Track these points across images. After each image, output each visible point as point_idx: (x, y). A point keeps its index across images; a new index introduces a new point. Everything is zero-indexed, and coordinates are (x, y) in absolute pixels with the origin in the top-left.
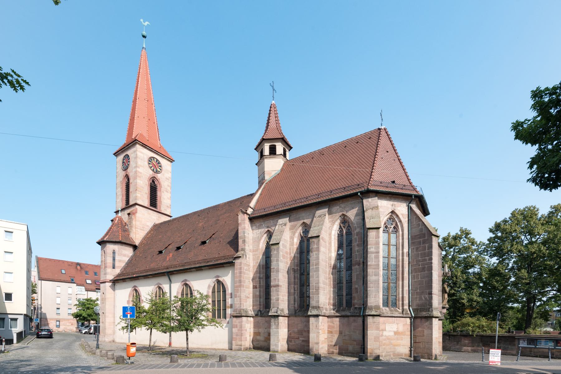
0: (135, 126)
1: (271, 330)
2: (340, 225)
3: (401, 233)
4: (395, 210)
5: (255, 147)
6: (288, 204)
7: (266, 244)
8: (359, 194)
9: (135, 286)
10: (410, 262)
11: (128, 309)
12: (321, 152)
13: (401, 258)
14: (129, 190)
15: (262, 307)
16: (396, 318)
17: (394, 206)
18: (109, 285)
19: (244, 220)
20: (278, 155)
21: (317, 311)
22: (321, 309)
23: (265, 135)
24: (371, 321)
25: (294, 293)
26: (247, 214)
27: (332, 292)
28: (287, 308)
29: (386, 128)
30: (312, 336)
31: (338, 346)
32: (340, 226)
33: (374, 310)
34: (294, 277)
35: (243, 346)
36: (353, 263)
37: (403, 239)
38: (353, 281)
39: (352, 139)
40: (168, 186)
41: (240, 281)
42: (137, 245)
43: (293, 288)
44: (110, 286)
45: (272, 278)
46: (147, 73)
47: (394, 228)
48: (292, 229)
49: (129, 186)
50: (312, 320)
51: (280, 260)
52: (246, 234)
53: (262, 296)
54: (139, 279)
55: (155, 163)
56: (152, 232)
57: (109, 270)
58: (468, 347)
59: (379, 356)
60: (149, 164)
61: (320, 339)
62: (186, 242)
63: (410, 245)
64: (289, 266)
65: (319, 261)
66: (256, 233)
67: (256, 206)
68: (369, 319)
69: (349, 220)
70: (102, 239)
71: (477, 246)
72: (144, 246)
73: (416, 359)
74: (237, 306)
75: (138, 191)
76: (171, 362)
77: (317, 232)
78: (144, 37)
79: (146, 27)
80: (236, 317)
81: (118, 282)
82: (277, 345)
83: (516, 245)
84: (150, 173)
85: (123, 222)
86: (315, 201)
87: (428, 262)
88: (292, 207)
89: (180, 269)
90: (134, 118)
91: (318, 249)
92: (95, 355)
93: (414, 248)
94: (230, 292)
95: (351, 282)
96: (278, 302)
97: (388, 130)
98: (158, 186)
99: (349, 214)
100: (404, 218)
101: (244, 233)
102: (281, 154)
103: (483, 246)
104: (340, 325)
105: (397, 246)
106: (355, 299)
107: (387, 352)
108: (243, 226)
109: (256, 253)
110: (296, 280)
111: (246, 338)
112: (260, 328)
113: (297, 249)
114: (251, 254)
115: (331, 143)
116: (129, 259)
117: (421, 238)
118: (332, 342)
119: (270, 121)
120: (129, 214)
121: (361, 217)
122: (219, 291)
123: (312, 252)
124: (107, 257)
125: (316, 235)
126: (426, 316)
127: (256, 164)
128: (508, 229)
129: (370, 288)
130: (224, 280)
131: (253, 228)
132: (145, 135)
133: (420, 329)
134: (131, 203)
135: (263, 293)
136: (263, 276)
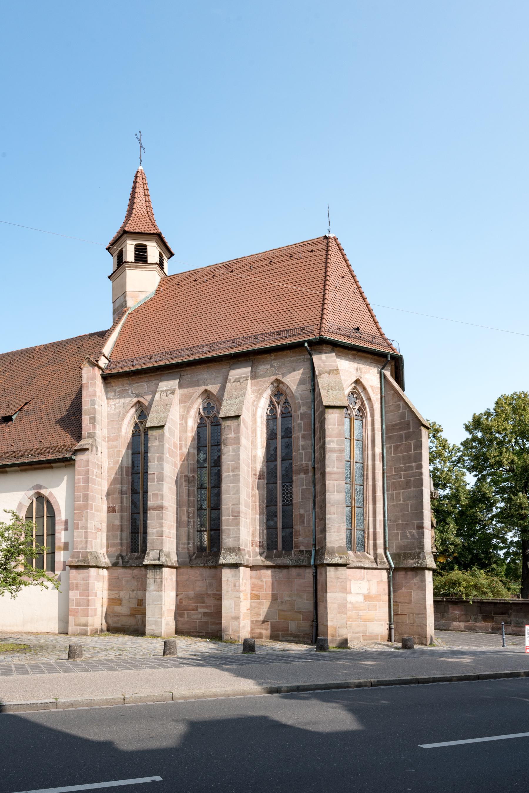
1: (147, 593)
2: (271, 398)
3: (369, 419)
4: (361, 377)
5: (108, 245)
7: (132, 428)
8: (306, 345)
10: (385, 471)
12: (227, 266)
13: (370, 463)
15: (124, 548)
16: (366, 571)
17: (359, 371)
19: (94, 378)
20: (150, 264)
21: (236, 556)
22: (243, 552)
24: (333, 576)
25: (188, 522)
26: (99, 367)
29: (337, 237)
30: (227, 604)
31: (270, 623)
32: (271, 401)
33: (337, 555)
34: (187, 491)
35: (91, 625)
36: (295, 467)
37: (373, 430)
38: (294, 502)
39: (280, 250)
41: (86, 497)
43: (186, 513)
47: (359, 410)
48: (185, 402)
50: (226, 573)
52: (96, 407)
53: (125, 527)
58: (459, 621)
59: (346, 641)
63: (384, 440)
64: (178, 470)
65: (239, 463)
66: (115, 405)
67: (112, 353)
68: (330, 571)
69: (288, 391)
71: (449, 452)
73: (406, 645)
74: (80, 546)
77: (234, 408)
80: (77, 567)
82: (158, 623)
83: (506, 452)
87: (416, 472)
88: (185, 360)
93: (390, 447)
94: (63, 518)
95: (292, 504)
96: (162, 539)
97: (339, 241)
99: (288, 380)
100: (374, 393)
101: (93, 403)
102: (156, 264)
103: (459, 452)
104: (273, 584)
105: (364, 441)
106: (300, 535)
107: (353, 633)
108: (90, 389)
109: (115, 443)
110: (192, 498)
111: (96, 609)
112: (122, 590)
113: (193, 440)
114: (105, 444)
115: (246, 253)
117: (402, 430)
121: (309, 387)
122: (40, 517)
123: (226, 445)
125: (233, 415)
126: (414, 567)
127: (109, 277)
128: (495, 427)
129: (330, 514)
130: (51, 493)
133: (404, 590)
135: (127, 521)
136: (128, 488)
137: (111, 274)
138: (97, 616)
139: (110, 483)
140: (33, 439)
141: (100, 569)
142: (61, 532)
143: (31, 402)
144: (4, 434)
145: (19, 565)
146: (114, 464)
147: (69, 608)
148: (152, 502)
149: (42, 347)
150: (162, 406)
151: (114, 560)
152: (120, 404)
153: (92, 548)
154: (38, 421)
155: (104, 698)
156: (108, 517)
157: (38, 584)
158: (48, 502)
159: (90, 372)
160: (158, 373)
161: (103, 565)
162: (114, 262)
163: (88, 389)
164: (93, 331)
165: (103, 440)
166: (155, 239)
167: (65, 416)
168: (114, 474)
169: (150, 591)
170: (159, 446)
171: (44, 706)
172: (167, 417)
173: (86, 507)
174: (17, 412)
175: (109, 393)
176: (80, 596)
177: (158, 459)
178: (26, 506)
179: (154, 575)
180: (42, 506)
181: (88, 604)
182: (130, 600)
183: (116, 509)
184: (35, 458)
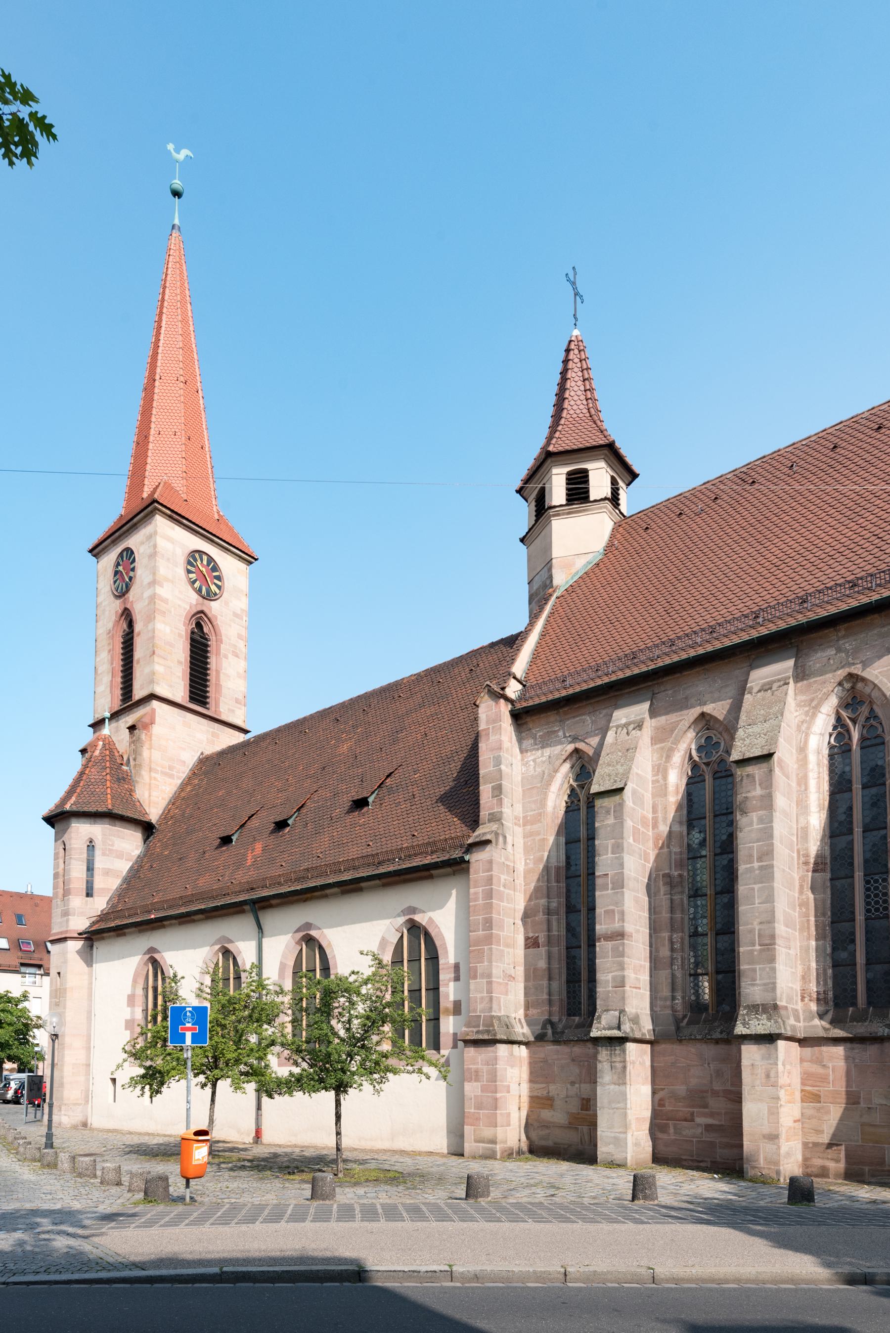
0: (149, 460)
2: (838, 713)
5: (518, 484)
6: (643, 658)
7: (566, 798)
9: (152, 950)
11: (185, 1014)
14: (132, 656)
15: (556, 1009)
18: (74, 946)
19: (498, 719)
20: (595, 501)
21: (769, 1019)
22: (783, 1012)
23: (554, 441)
25: (672, 959)
26: (507, 699)
27: (813, 955)
28: (649, 1012)
31: (843, 1148)
32: (839, 719)
34: (668, 902)
35: (502, 1142)
39: (855, 420)
40: (240, 637)
41: (489, 924)
42: (154, 821)
43: (667, 942)
44: (78, 952)
45: (599, 911)
46: (183, 302)
48: (662, 741)
49: (132, 644)
51: (625, 845)
52: (503, 767)
54: (164, 927)
55: (204, 570)
56: (196, 781)
57: (77, 901)
60: (189, 572)
61: (781, 1120)
62: (302, 806)
64: (650, 866)
65: (772, 844)
66: (534, 760)
67: (528, 672)
69: (875, 694)
70: (57, 806)
72: (174, 824)
75: (159, 656)
76: (313, 1196)
77: (761, 741)
78: (177, 194)
79: (181, 164)
80: (476, 1043)
81: (103, 939)
82: (620, 1143)
84: (190, 599)
85: (117, 754)
86: (745, 637)
89: (293, 889)
90: (147, 437)
91: (768, 802)
92: (54, 1171)
96: (624, 992)
98: (213, 638)
99: (876, 672)
101: (498, 761)
102: (606, 499)
104: (848, 1073)
108: (493, 738)
109: (536, 827)
110: (678, 916)
111: (509, 1114)
113: (679, 808)
114: (519, 830)
116: (132, 867)
118: (819, 1132)
119: (567, 395)
120: (132, 728)
122: (414, 960)
123: (744, 813)
124: (73, 862)
127: (522, 540)
131: (524, 747)
132: (179, 485)
134: (138, 693)
135: (560, 960)
136: (559, 903)
138: (511, 1127)
139: (528, 897)
140: (401, 832)
141: (514, 1046)
143: (397, 771)
146: (534, 864)
147: (463, 1112)
148: (603, 926)
150: (620, 754)
151: (538, 1029)
152: (544, 759)
153: (500, 1010)
155: (531, 1270)
156: (526, 956)
158: (427, 935)
159: (492, 709)
160: (612, 694)
163: (489, 738)
164: (495, 639)
165: (516, 824)
167: (451, 788)
168: (535, 880)
169: (603, 1085)
171: (431, 1277)
172: (629, 772)
173: (489, 940)
174: (376, 790)
176: (482, 1091)
177: (613, 848)
178: (393, 943)
182: (567, 1099)
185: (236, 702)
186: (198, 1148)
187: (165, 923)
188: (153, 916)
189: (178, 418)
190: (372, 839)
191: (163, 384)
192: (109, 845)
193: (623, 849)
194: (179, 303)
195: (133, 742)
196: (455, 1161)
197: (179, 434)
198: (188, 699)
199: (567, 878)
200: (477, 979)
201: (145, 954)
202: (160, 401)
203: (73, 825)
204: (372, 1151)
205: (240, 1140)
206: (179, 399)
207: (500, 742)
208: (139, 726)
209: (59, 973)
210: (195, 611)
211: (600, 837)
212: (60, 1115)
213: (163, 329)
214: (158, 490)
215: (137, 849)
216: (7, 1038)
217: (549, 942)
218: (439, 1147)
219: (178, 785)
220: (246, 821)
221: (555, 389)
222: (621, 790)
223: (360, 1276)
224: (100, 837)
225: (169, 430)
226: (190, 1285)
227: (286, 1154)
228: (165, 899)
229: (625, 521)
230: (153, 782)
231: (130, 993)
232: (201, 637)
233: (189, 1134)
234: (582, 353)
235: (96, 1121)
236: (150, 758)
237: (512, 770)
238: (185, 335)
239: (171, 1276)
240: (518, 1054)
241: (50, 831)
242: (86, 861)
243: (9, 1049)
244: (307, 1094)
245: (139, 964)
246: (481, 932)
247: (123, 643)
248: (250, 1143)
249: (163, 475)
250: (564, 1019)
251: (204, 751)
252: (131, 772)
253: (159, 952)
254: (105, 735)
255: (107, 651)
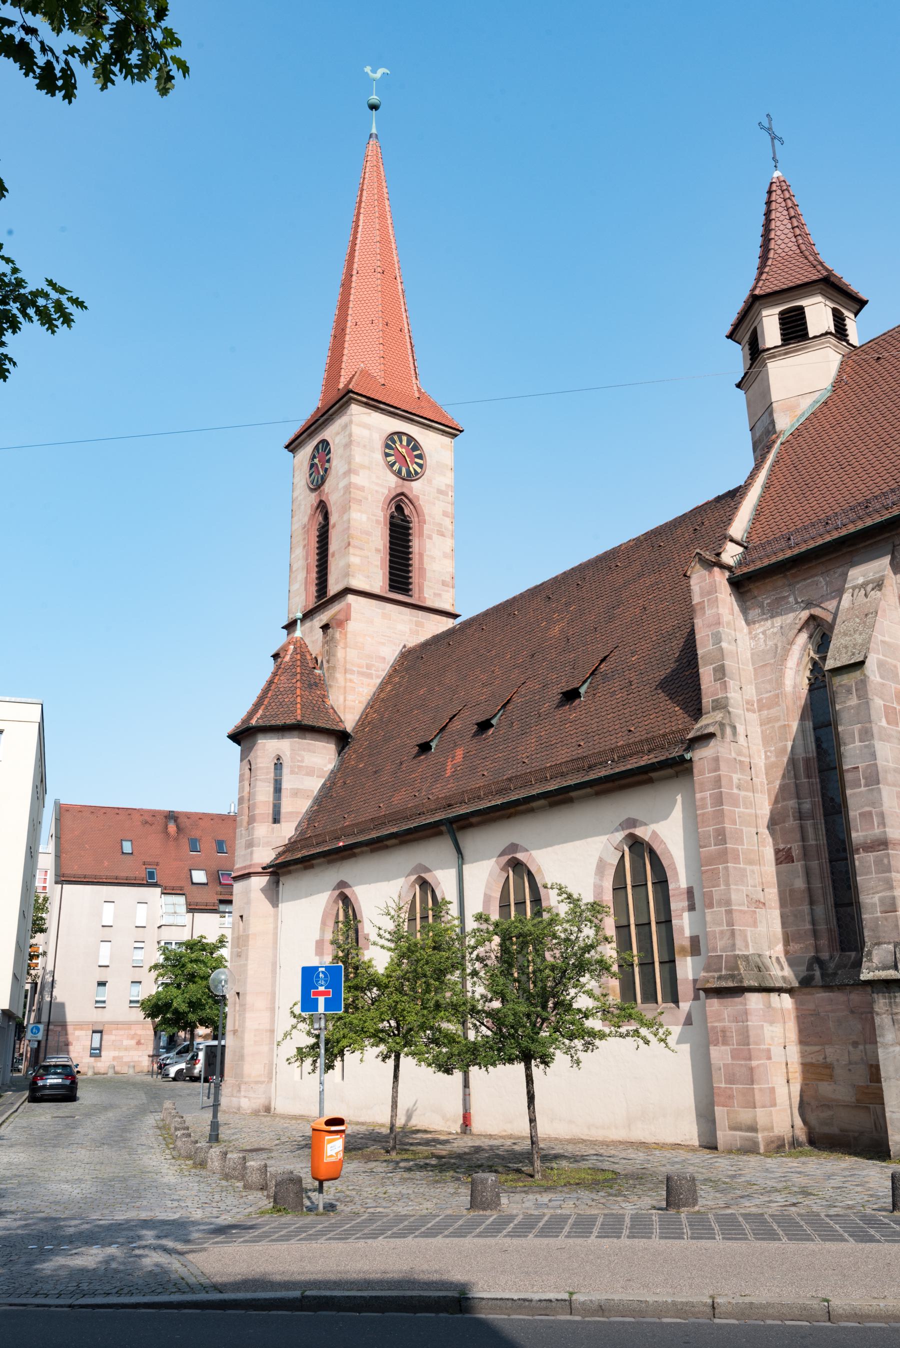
0: (346, 352)
5: (728, 329)
6: (878, 506)
7: (808, 673)
11: (318, 976)
14: (327, 550)
15: (824, 942)
18: (259, 882)
19: (713, 590)
26: (723, 566)
35: (765, 1129)
40: (445, 514)
41: (721, 836)
42: (349, 729)
44: (262, 890)
46: (381, 200)
51: (875, 730)
52: (724, 645)
53: (818, 894)
55: (403, 451)
60: (387, 455)
66: (764, 633)
72: (371, 731)
74: (720, 944)
75: (355, 547)
78: (374, 107)
81: (290, 872)
85: (308, 657)
89: (493, 803)
90: (344, 330)
94: (683, 884)
98: (415, 519)
102: (827, 333)
108: (709, 612)
109: (774, 712)
111: (772, 1090)
114: (753, 717)
116: (324, 784)
120: (325, 627)
122: (639, 886)
124: (259, 783)
127: (739, 386)
130: (654, 833)
132: (376, 371)
134: (333, 588)
135: (822, 878)
136: (813, 804)
137: (740, 379)
138: (778, 1108)
139: (773, 798)
140: (616, 727)
141: (772, 994)
142: (682, 915)
143: (613, 654)
144: (567, 726)
145: (581, 994)
146: (777, 757)
147: (712, 1088)
148: (860, 834)
149: (631, 544)
150: (857, 620)
151: (803, 970)
152: (775, 630)
153: (747, 946)
154: (625, 689)
155: (669, 1300)
156: (778, 874)
157: (627, 1035)
158: (652, 852)
159: (705, 580)
160: (845, 550)
161: (778, 985)
162: (744, 356)
163: (704, 613)
164: (721, 492)
165: (748, 710)
166: (818, 289)
167: (673, 671)
168: (780, 777)
169: (885, 1046)
170: (859, 705)
171: (546, 1308)
172: (869, 642)
173: (723, 856)
174: (588, 678)
175: (751, 612)
176: (733, 1058)
177: (860, 735)
178: (612, 865)
179: (891, 1006)
180: (642, 861)
181: (751, 1077)
182: (851, 1067)
183: (794, 855)
184: (618, 765)
185: (443, 585)
186: (330, 1141)
187: (356, 851)
188: (341, 844)
189: (375, 307)
190: (583, 737)
191: (360, 278)
192: (298, 761)
193: (872, 735)
194: (376, 202)
195: (327, 642)
196: (707, 1155)
197: (376, 321)
198: (388, 588)
199: (820, 772)
200: (713, 908)
201: (334, 889)
202: (357, 294)
203: (259, 741)
204: (593, 1143)
205: (446, 1129)
206: (376, 289)
207: (718, 616)
208: (333, 624)
209: (241, 917)
210: (394, 494)
211: (843, 721)
212: (239, 1097)
213: (360, 227)
214: (354, 380)
215: (330, 763)
216: (199, 996)
217: (805, 855)
218: (687, 1137)
219: (377, 685)
220: (447, 723)
221: (760, 230)
222: (862, 663)
223: (460, 1305)
224: (288, 753)
225: (366, 319)
226: (266, 1312)
227: (492, 1148)
228: (357, 821)
229: (855, 352)
230: (348, 684)
231: (318, 939)
232: (402, 520)
233: (321, 1124)
234: (786, 192)
235: (281, 1106)
236: (345, 658)
237: (737, 647)
238: (383, 229)
239: (247, 1300)
240: (779, 1006)
241: (237, 749)
242: (272, 781)
243: (202, 1010)
244: (484, 1069)
245: (328, 902)
246: (713, 848)
247: (318, 536)
248: (457, 1134)
249: (359, 363)
250: (837, 955)
251: (407, 643)
252: (324, 676)
253: (350, 887)
254: (297, 638)
255: (302, 547)
